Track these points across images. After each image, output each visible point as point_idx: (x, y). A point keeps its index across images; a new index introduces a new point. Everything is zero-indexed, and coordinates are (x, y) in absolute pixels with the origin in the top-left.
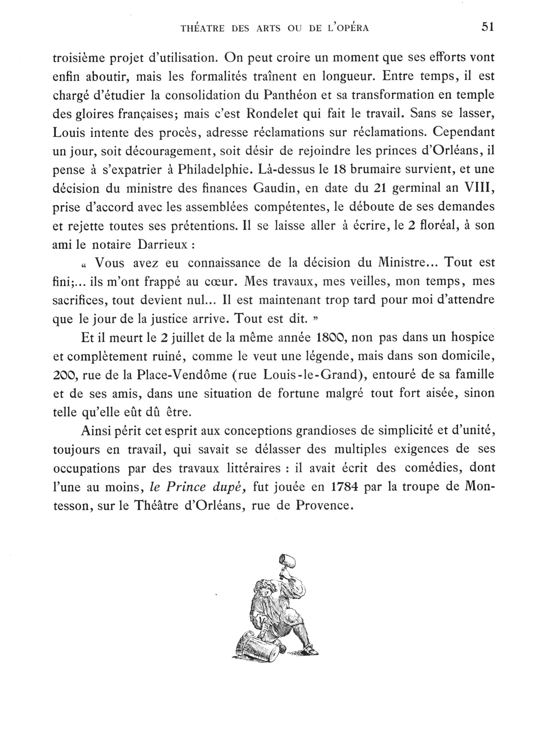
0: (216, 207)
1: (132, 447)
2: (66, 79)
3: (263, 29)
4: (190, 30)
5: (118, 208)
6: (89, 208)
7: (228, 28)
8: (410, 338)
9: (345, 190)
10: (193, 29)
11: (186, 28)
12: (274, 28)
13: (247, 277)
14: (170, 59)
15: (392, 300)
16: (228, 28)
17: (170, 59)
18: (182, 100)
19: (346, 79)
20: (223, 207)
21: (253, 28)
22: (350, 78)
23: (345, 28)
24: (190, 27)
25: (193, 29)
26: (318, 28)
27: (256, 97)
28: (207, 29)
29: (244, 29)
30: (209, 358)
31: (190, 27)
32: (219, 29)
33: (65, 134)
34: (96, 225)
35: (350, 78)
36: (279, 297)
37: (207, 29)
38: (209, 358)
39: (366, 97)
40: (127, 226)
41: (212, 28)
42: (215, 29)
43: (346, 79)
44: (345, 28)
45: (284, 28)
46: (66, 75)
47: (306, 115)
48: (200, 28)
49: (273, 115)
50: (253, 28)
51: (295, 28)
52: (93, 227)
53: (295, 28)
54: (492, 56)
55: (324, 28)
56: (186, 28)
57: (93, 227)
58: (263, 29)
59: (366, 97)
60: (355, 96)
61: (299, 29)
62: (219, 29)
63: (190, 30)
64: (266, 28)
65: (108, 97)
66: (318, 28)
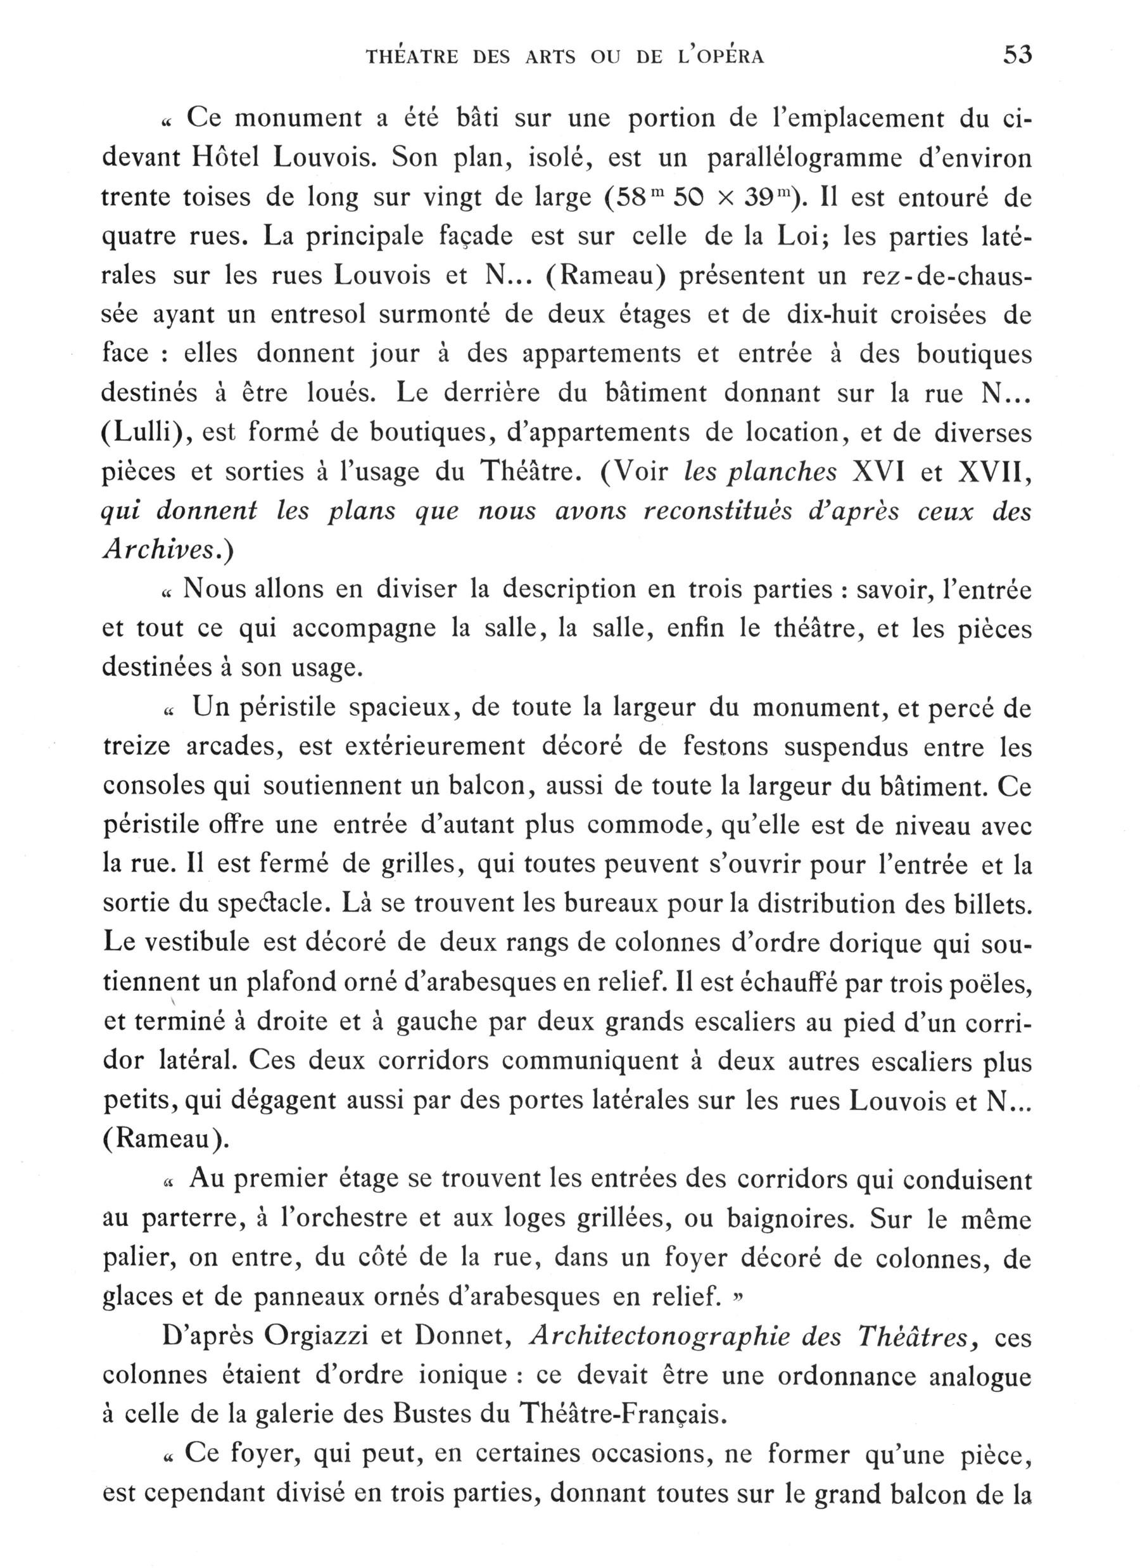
2: (695, 632)
3: (539, 59)
6: (428, 826)
8: (570, 1260)
26: (654, 57)
33: (300, 159)
36: (541, 1448)
41: (431, 57)
58: (539, 59)
66: (654, 57)
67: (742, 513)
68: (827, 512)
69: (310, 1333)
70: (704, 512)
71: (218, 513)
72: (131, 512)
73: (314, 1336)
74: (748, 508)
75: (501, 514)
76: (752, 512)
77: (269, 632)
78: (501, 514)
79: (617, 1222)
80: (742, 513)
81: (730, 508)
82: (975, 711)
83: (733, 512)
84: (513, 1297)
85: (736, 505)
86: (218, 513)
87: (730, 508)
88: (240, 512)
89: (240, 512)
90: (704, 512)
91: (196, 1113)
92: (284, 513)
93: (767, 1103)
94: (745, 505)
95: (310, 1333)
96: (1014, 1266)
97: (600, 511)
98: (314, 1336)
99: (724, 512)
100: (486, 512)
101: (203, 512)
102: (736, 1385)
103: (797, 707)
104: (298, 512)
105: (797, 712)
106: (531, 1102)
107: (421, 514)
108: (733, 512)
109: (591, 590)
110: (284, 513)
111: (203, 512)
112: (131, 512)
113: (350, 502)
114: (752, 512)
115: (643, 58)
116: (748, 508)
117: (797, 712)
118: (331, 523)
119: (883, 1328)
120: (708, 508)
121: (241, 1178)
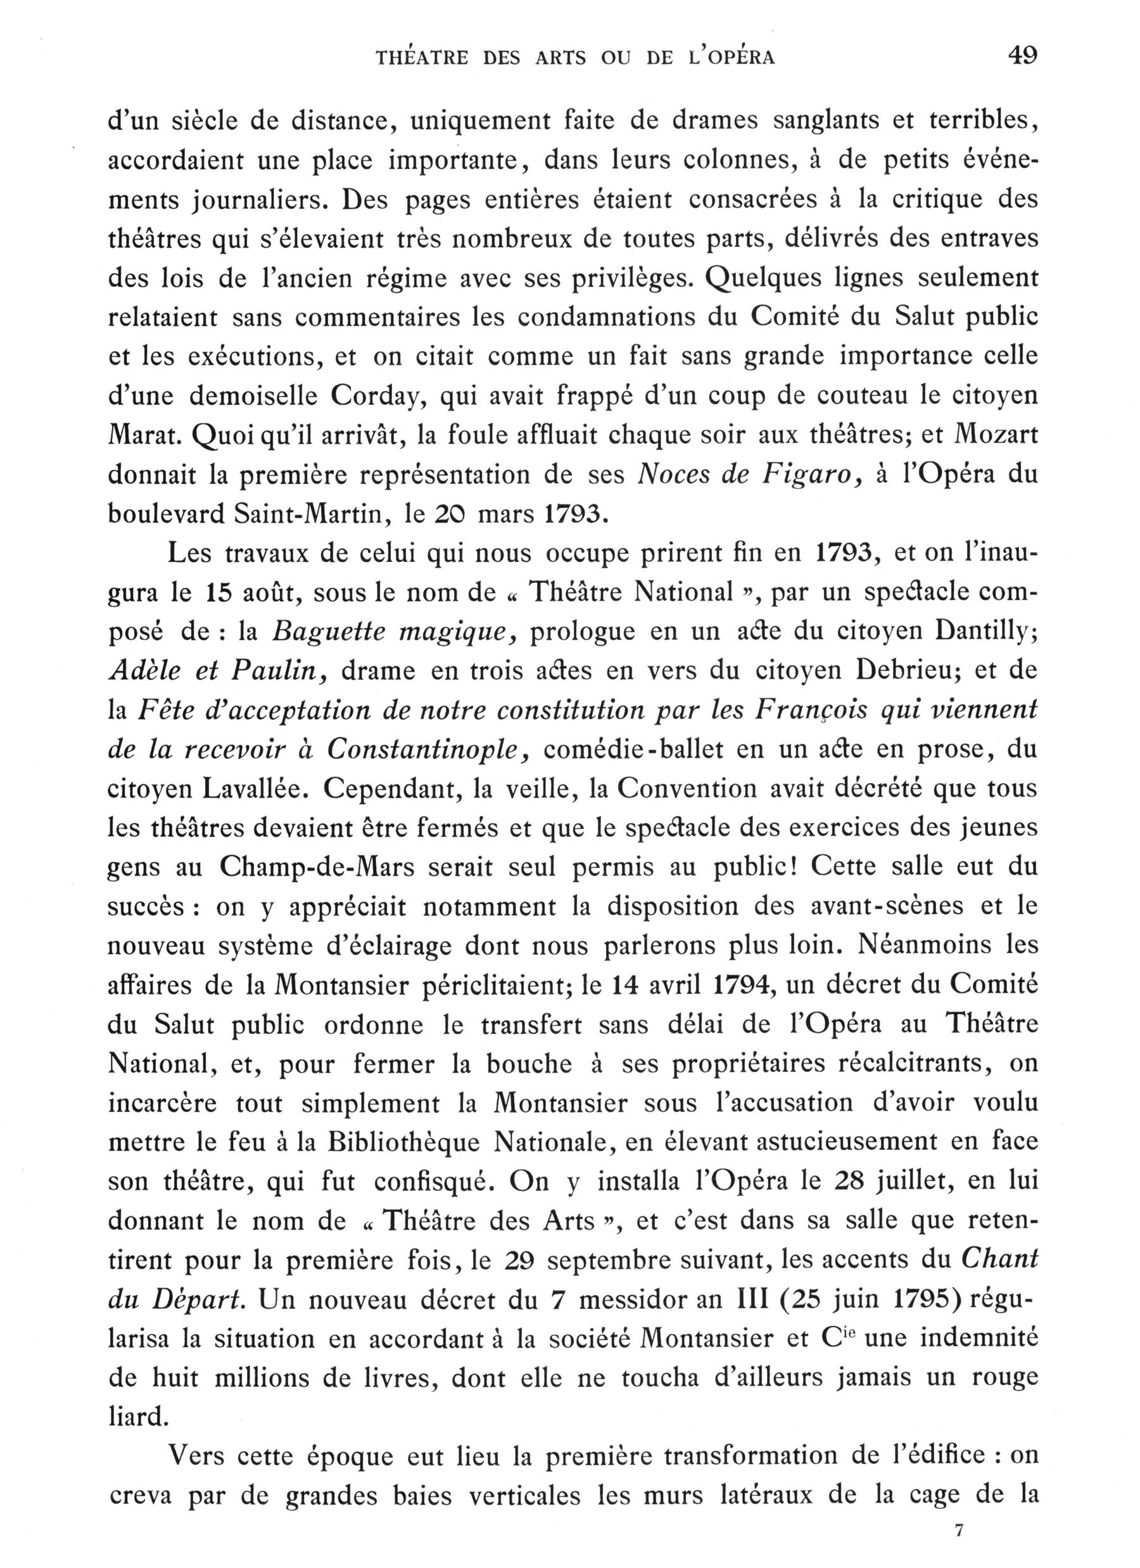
0: (497, 239)
1: (673, 1450)
2: (417, 1186)
3: (549, 60)
4: (396, 61)
5: (564, 752)
7: (476, 57)
9: (870, 870)
10: (400, 58)
11: (387, 58)
12: (573, 57)
13: (647, 1329)
14: (991, 632)
15: (130, 516)
16: (476, 57)
17: (991, 632)
18: (724, 209)
19: (607, 636)
20: (1003, 317)
21: (529, 57)
22: (615, 635)
23: (726, 57)
24: (396, 54)
25: (400, 58)
26: (664, 58)
27: (731, 320)
28: (430, 58)
29: (510, 58)
30: (1014, 596)
31: (396, 54)
32: (456, 59)
34: (276, 1453)
35: (615, 635)
37: (430, 58)
38: (1014, 596)
39: (932, 359)
40: (860, 396)
41: (441, 57)
42: (448, 59)
43: (607, 636)
44: (726, 57)
45: (593, 57)
46: (416, 1177)
47: (549, 832)
48: (417, 57)
49: (803, 357)
50: (529, 57)
51: (618, 57)
52: (271, 1458)
53: (618, 57)
54: (989, 863)
55: (680, 58)
56: (387, 58)
57: (271, 1458)
58: (549, 60)
59: (932, 359)
60: (489, 1027)
61: (624, 59)
62: (456, 59)
63: (396, 61)
64: (556, 58)
65: (600, 203)
66: (664, 58)
67: (570, 712)
68: (224, 712)
69: (400, 276)
70: (532, 712)
71: (998, 712)
72: (911, 711)
73: (404, 278)
74: (575, 708)
75: (443, 714)
76: (579, 712)
77: (408, 557)
78: (443, 714)
79: (915, 1184)
80: (570, 712)
81: (557, 708)
82: (174, 1105)
83: (561, 712)
84: (358, 1460)
85: (564, 704)
86: (998, 712)
87: (557, 708)
88: (975, 711)
89: (975, 711)
90: (532, 712)
91: (944, 801)
92: (718, 712)
93: (684, 240)
94: (572, 704)
95: (400, 276)
96: (796, 244)
97: (630, 711)
98: (404, 278)
99: (552, 712)
100: (428, 712)
101: (983, 711)
102: (682, 405)
103: (541, 1103)
104: (733, 711)
105: (541, 1108)
106: (442, 162)
107: (887, 713)
108: (561, 712)
109: (588, 1261)
110: (718, 712)
111: (983, 711)
112: (911, 711)
113: (502, 740)
114: (579, 712)
115: (654, 59)
116: (575, 708)
117: (541, 1108)
118: (235, 678)
119: (988, 1250)
120: (536, 708)
121: (648, 553)
